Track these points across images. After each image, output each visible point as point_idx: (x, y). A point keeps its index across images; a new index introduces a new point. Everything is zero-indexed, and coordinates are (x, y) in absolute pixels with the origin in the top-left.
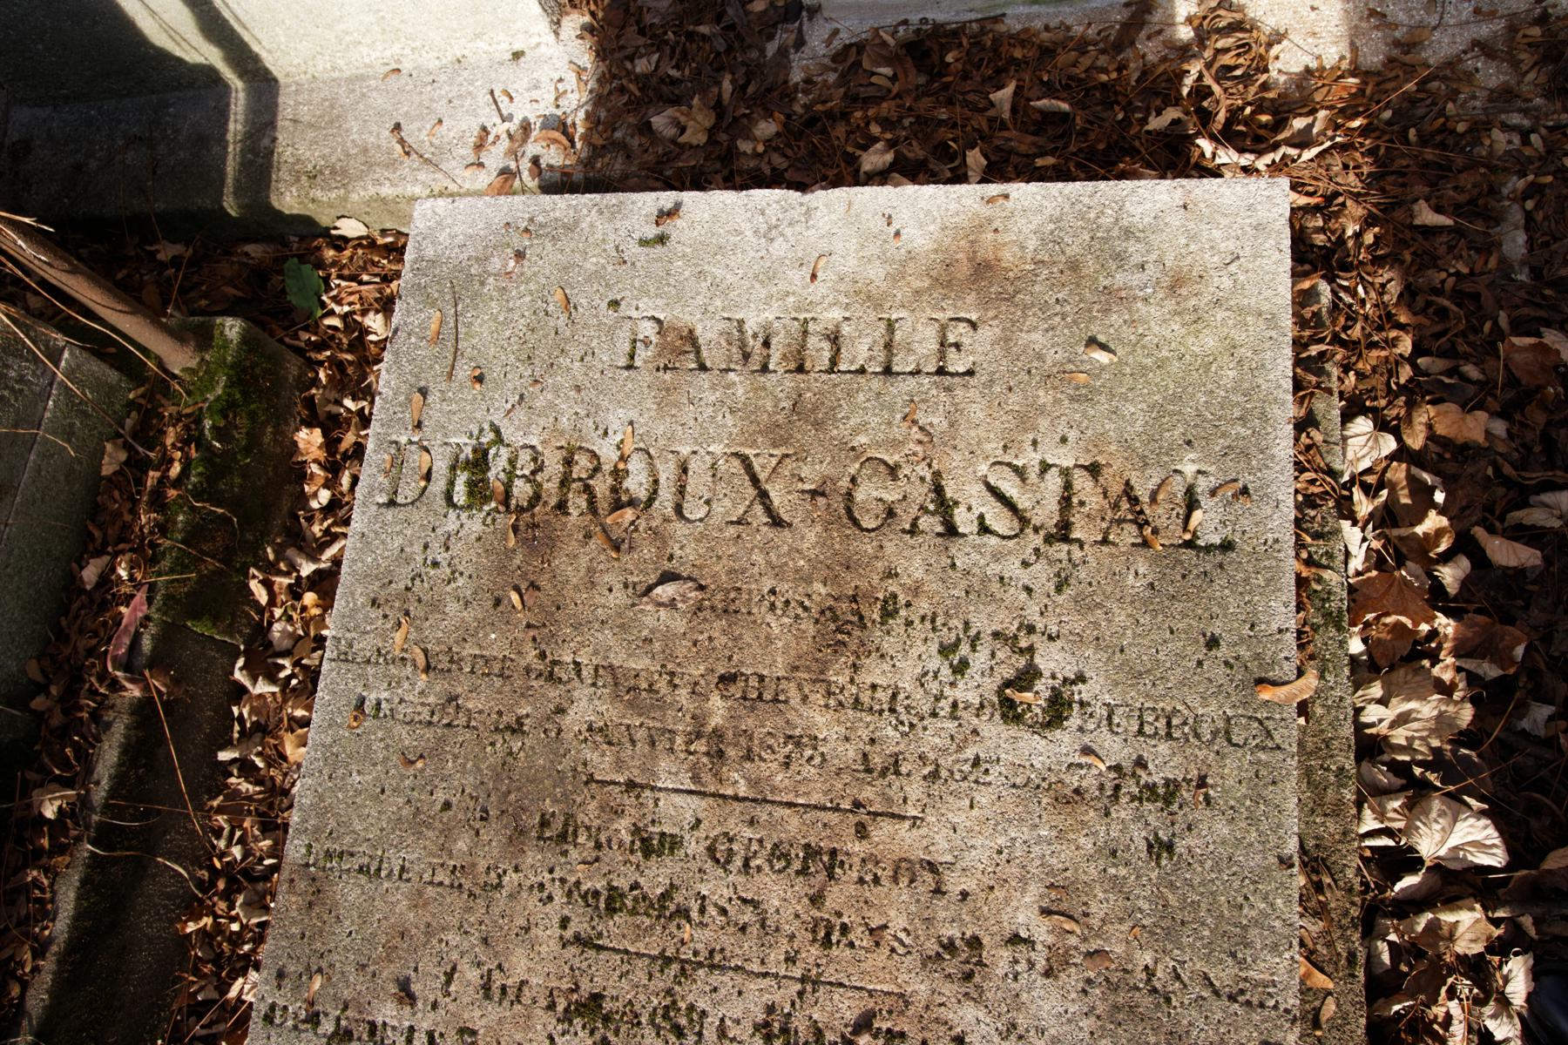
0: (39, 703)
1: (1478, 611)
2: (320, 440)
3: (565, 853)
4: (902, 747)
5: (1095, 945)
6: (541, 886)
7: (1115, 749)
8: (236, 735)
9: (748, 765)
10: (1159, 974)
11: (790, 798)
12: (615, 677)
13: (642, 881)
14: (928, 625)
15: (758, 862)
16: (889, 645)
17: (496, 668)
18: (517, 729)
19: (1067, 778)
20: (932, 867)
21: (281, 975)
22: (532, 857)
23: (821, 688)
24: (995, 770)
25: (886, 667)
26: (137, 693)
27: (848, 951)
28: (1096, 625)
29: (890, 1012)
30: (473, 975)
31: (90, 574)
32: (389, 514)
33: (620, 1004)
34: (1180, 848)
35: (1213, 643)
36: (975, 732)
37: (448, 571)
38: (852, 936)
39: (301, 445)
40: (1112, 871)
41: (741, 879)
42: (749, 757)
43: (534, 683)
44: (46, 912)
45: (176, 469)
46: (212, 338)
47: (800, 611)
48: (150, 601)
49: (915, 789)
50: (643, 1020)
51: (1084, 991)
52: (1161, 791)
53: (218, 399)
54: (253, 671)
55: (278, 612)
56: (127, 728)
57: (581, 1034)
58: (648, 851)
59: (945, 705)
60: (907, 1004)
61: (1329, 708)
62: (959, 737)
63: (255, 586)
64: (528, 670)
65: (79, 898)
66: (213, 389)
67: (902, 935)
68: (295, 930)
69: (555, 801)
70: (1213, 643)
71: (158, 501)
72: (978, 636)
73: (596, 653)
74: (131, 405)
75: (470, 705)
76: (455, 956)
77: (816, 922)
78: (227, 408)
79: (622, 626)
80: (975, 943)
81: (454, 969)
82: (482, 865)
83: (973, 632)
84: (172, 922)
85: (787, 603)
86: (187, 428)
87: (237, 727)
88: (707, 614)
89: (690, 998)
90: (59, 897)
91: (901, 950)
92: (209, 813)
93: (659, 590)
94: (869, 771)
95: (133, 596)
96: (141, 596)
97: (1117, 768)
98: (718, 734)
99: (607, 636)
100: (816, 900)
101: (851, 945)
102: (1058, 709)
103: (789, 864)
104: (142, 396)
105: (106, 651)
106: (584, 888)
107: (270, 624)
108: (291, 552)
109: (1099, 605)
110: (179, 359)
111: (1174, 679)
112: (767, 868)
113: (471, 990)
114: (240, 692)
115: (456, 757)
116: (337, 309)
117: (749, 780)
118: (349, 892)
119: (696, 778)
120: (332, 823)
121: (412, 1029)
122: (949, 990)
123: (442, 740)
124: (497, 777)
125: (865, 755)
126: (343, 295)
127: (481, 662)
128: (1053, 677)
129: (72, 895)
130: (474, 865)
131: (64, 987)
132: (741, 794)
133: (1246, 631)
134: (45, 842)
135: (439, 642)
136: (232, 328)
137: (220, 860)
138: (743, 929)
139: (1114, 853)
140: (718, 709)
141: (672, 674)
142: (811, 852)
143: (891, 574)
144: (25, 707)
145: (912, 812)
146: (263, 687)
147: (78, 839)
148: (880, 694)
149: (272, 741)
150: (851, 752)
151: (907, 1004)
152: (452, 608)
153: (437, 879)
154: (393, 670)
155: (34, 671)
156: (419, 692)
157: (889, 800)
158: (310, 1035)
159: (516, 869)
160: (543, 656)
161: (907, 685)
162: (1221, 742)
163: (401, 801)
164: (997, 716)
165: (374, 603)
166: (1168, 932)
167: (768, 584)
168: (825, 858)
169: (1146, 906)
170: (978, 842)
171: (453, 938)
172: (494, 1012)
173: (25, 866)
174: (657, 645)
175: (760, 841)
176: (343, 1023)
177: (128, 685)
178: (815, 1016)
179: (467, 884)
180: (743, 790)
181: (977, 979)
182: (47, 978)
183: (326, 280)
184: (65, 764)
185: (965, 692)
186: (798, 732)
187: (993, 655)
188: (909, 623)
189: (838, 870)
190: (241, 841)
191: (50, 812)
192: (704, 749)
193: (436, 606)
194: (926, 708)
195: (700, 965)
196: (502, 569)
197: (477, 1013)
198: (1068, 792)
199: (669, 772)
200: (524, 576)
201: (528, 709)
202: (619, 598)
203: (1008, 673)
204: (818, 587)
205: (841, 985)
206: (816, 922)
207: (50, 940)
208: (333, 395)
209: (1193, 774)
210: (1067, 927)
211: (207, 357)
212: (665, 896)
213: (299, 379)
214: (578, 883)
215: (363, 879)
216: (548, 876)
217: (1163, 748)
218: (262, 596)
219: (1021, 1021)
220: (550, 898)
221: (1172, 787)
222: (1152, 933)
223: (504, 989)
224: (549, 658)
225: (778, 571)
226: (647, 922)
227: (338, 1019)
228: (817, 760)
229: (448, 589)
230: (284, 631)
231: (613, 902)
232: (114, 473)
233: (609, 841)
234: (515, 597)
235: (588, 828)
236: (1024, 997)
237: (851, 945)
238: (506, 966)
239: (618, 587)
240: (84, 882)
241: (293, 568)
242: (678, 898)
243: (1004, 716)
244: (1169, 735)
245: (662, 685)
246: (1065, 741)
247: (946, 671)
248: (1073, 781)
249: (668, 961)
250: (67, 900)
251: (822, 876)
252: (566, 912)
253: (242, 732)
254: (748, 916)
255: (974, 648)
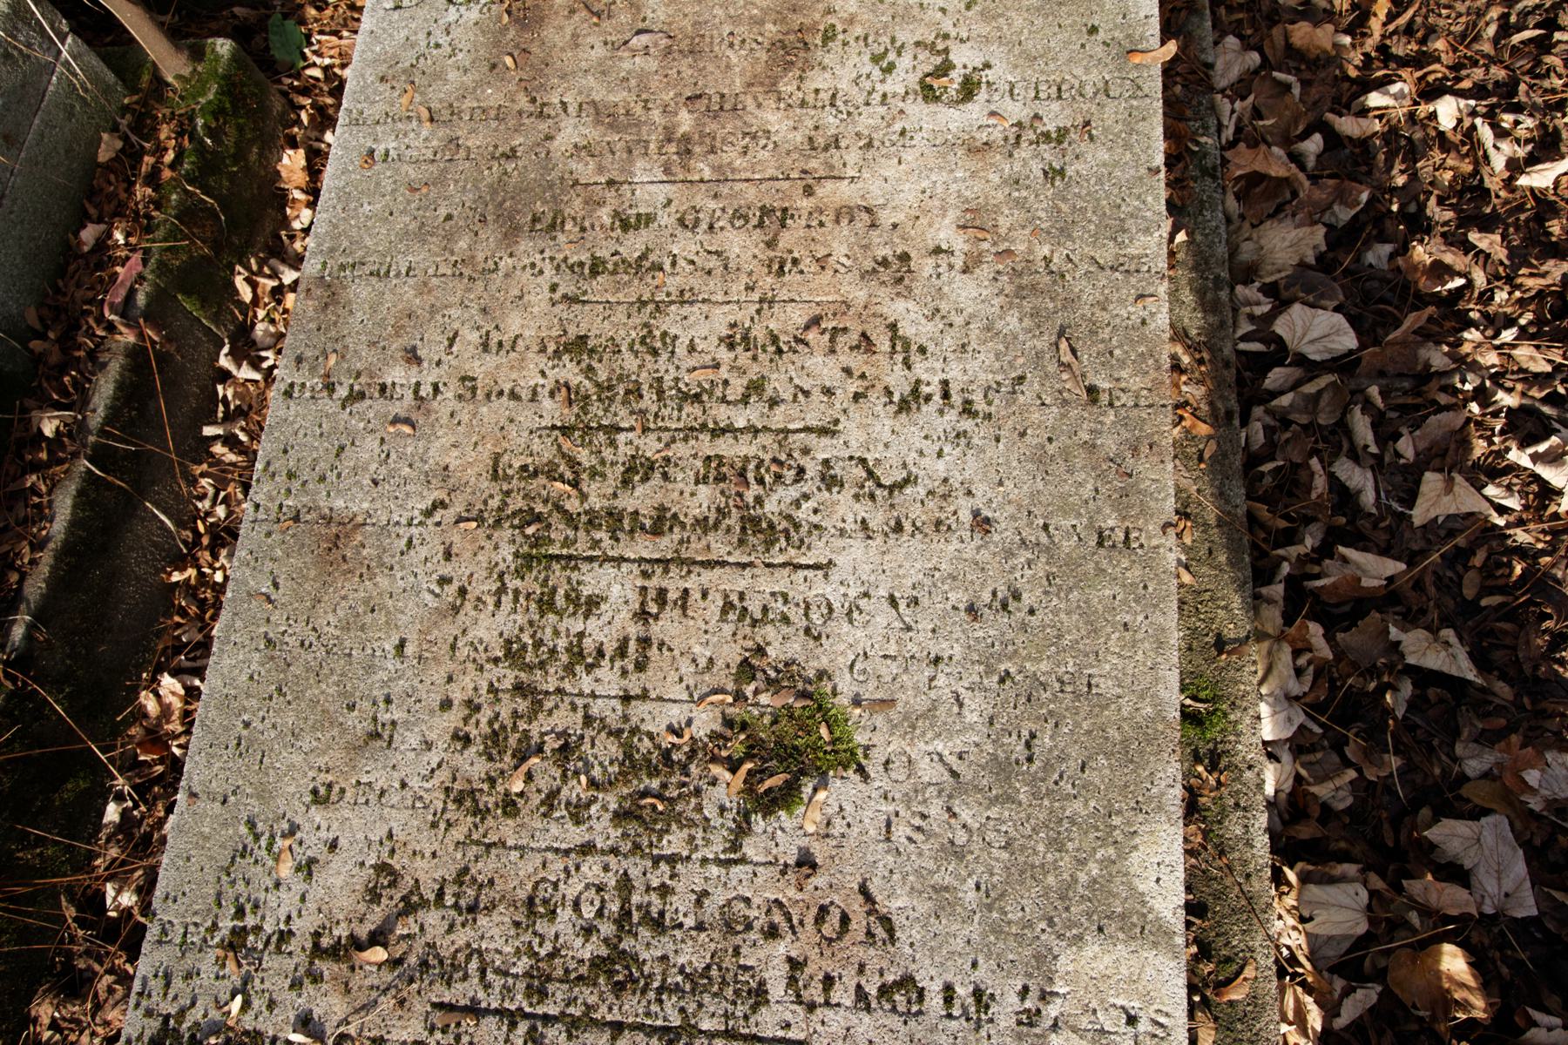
0: (36, 345)
1: (1330, 177)
2: (303, 163)
3: (554, 238)
4: (841, 129)
5: (1003, 246)
6: (533, 265)
7: (1016, 111)
8: (220, 415)
9: (711, 157)
10: (1055, 260)
11: (748, 175)
12: (596, 109)
13: (621, 250)
14: (862, 43)
15: (721, 224)
16: (828, 60)
17: (493, 113)
18: (511, 155)
19: (978, 136)
20: (868, 210)
21: (299, 360)
22: (525, 245)
23: (774, 96)
24: (918, 137)
25: (826, 75)
26: (131, 338)
27: (799, 276)
28: (999, 29)
29: (835, 314)
30: (474, 337)
31: (89, 234)
32: (396, 15)
33: (603, 340)
34: (1070, 171)
35: (1093, 30)
36: (902, 112)
37: (449, 49)
38: (801, 267)
39: (284, 174)
40: (1016, 194)
41: (707, 237)
42: (713, 151)
43: (526, 121)
44: (43, 514)
45: (170, 156)
46: (204, 54)
47: (754, 45)
48: (145, 262)
49: (853, 157)
50: (623, 349)
51: (995, 279)
52: (1054, 135)
53: (210, 102)
54: (237, 356)
55: (261, 313)
56: (122, 366)
57: (569, 365)
58: (626, 226)
59: (877, 97)
60: (848, 307)
61: (1206, 236)
62: (888, 118)
63: (239, 282)
64: (520, 113)
65: (75, 506)
66: (205, 94)
67: (844, 260)
68: (313, 326)
69: (545, 202)
70: (1093, 30)
71: (153, 179)
72: (903, 46)
73: (580, 93)
74: (125, 109)
75: (469, 143)
76: (456, 325)
77: (771, 260)
78: (217, 112)
79: (603, 73)
80: (905, 258)
81: (456, 334)
82: (480, 256)
83: (898, 44)
84: (158, 571)
85: (743, 41)
86: (181, 124)
87: (221, 408)
88: (676, 55)
89: (664, 327)
90: (56, 504)
91: (843, 270)
92: (193, 482)
93: (635, 40)
94: (814, 149)
95: (128, 258)
96: (137, 257)
97: (1019, 124)
98: (686, 138)
99: (591, 80)
100: (771, 244)
101: (802, 272)
102: (969, 90)
103: (747, 222)
104: (136, 103)
105: (103, 301)
106: (571, 261)
107: (253, 325)
108: (273, 261)
109: (1000, 15)
110: (171, 63)
111: (1065, 55)
112: (729, 226)
113: (471, 348)
114: (225, 376)
115: (456, 182)
116: (318, 61)
117: (713, 168)
118: (360, 291)
119: (667, 171)
120: (345, 244)
121: (418, 384)
122: (884, 293)
123: (445, 171)
124: (494, 192)
125: (810, 139)
126: (324, 50)
127: (478, 111)
128: (965, 67)
129: (69, 502)
130: (473, 257)
131: (57, 583)
132: (706, 178)
133: (1119, 19)
134: (44, 456)
135: (441, 101)
136: (223, 47)
137: (204, 520)
138: (709, 273)
139: (1017, 182)
140: (685, 121)
141: (646, 101)
142: (766, 211)
143: (829, 11)
144: (25, 344)
145: (851, 173)
146: (246, 373)
147: (75, 455)
148: (822, 95)
149: (257, 418)
150: (799, 137)
151: (848, 307)
152: (452, 75)
153: (441, 271)
154: (400, 125)
155: (32, 318)
156: (422, 139)
157: (832, 167)
158: (327, 400)
159: (511, 255)
160: (533, 100)
161: (844, 85)
162: (1101, 97)
163: (407, 219)
164: (920, 99)
165: (383, 79)
166: (1062, 230)
167: (727, 29)
168: (778, 214)
169: (1043, 215)
170: (908, 186)
171: (455, 312)
172: (491, 360)
173: (25, 472)
174: (633, 82)
175: (723, 210)
176: (356, 388)
177: (123, 329)
178: (771, 326)
179: (467, 272)
180: (707, 174)
181: (907, 281)
182: (44, 569)
183: (308, 36)
184: (64, 392)
185: (894, 85)
186: (754, 129)
187: (915, 57)
188: (845, 44)
189: (789, 222)
190: (226, 501)
191: (49, 429)
192: (674, 150)
193: (439, 76)
194: (861, 100)
195: (673, 302)
196: (497, 44)
197: (477, 363)
198: (978, 144)
199: (645, 172)
200: (517, 46)
201: (522, 140)
202: (600, 51)
203: (929, 68)
204: (769, 26)
205: (793, 301)
206: (771, 260)
207: (48, 539)
208: (314, 134)
209: (1080, 120)
210: (980, 236)
211: (199, 69)
212: (643, 257)
213: (283, 115)
214: (565, 259)
215: (374, 280)
216: (538, 256)
217: (1055, 106)
218: (246, 294)
219: (944, 306)
220: (541, 272)
221: (1062, 133)
222: (1049, 233)
223: (500, 344)
224: (539, 101)
225: (735, 20)
226: (626, 278)
227: (352, 386)
228: (771, 146)
229: (450, 62)
230: (266, 331)
231: (596, 268)
232: (111, 160)
233: (593, 226)
234: (509, 61)
235: (574, 219)
236: (946, 289)
237: (802, 272)
238: (502, 326)
239: (598, 45)
240: (81, 493)
241: (275, 275)
242: (653, 257)
243: (925, 98)
244: (1059, 97)
245: (638, 110)
246: (975, 111)
247: (877, 73)
248: (983, 136)
249: (644, 304)
250: (64, 507)
251: (775, 227)
252: (555, 280)
253: (227, 412)
254: (713, 263)
255: (899, 54)
